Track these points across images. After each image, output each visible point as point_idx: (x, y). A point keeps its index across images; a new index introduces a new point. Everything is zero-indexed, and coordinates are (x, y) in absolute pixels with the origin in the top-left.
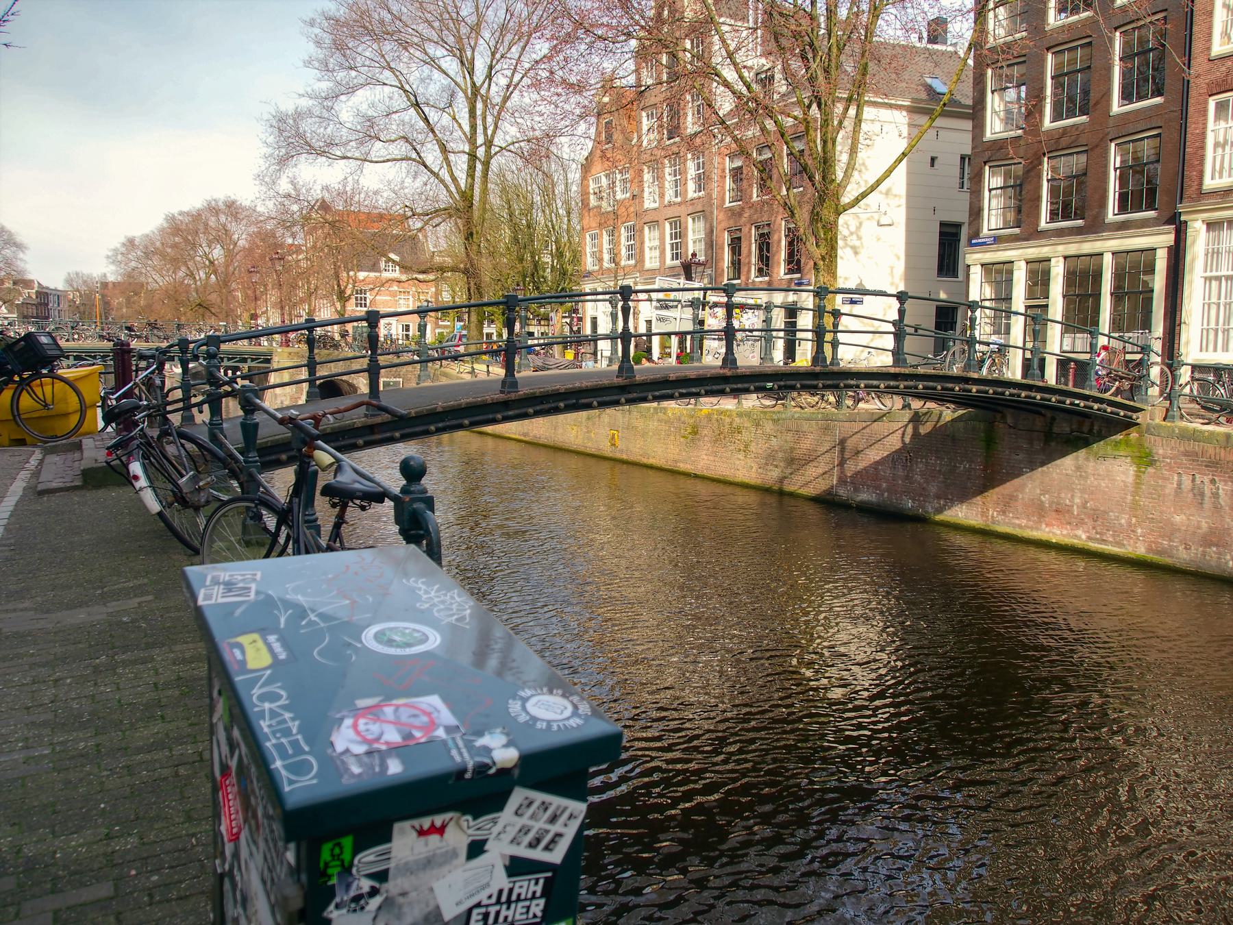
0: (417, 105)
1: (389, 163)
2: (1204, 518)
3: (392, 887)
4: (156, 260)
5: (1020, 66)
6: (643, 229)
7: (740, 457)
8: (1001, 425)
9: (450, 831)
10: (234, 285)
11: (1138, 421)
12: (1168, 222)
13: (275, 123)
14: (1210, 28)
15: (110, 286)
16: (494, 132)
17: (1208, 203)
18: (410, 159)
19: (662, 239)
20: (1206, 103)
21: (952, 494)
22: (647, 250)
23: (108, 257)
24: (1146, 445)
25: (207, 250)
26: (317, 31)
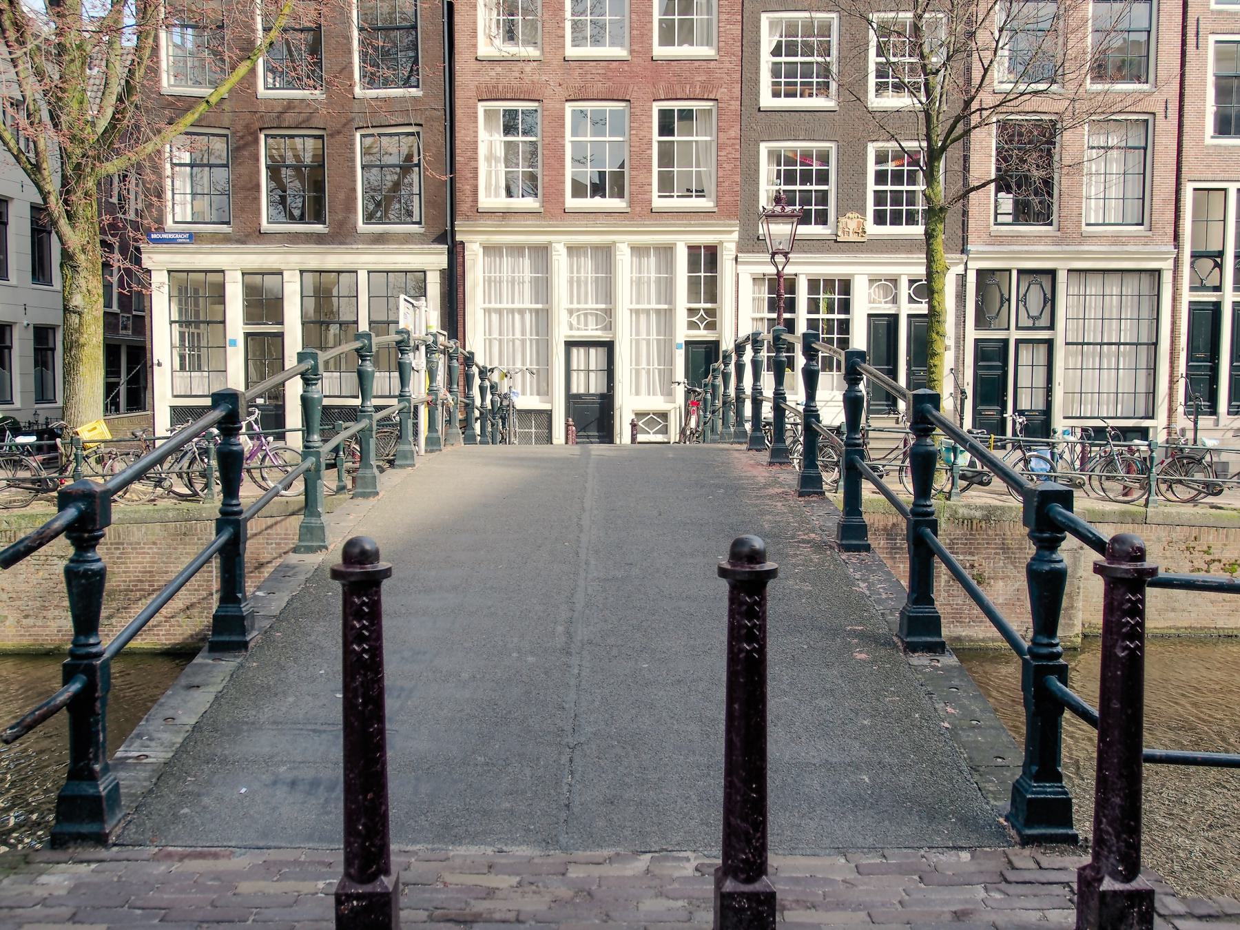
12: (440, 239)
17: (486, 224)
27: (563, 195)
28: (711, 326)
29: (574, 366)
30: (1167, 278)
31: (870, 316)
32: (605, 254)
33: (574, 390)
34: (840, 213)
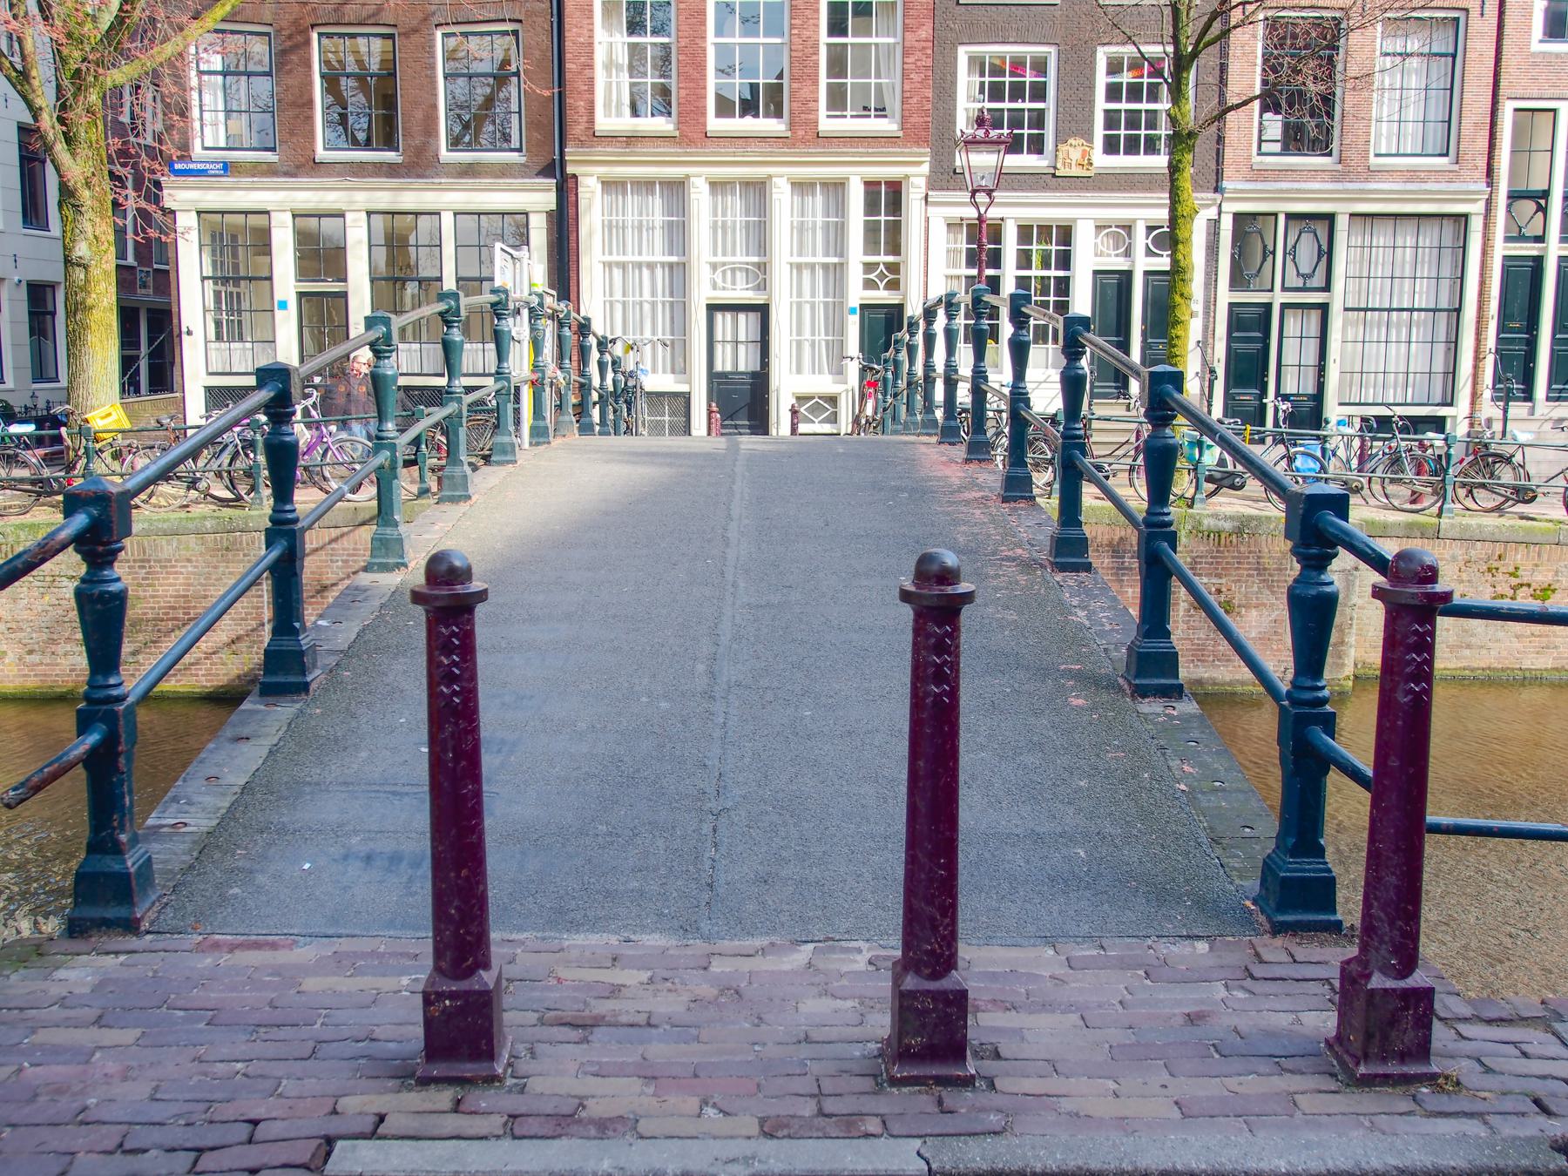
17: (601, 152)
27: (703, 112)
28: (894, 285)
29: (719, 336)
30: (1476, 225)
31: (1096, 273)
33: (719, 368)
34: (1060, 139)
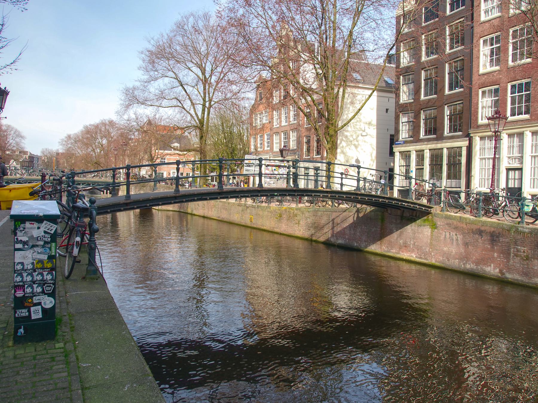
0: (182, 85)
1: (169, 108)
2: (454, 248)
3: (26, 230)
4: (79, 144)
5: (413, 75)
6: (273, 136)
7: (296, 226)
8: (386, 213)
9: (34, 224)
10: (111, 155)
11: (431, 212)
13: (125, 92)
14: (479, 63)
15: (60, 154)
16: (213, 96)
18: (179, 106)
19: (280, 139)
20: (478, 91)
21: (370, 240)
22: (274, 144)
23: (59, 142)
24: (434, 221)
25: (100, 140)
26: (143, 56)
29: (510, 177)
32: (521, 135)
33: (510, 186)
